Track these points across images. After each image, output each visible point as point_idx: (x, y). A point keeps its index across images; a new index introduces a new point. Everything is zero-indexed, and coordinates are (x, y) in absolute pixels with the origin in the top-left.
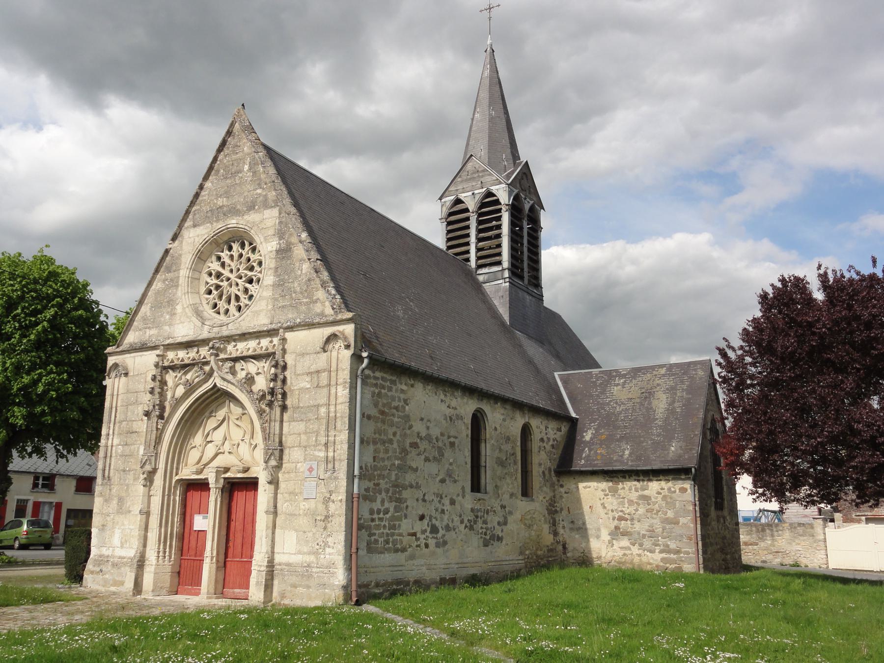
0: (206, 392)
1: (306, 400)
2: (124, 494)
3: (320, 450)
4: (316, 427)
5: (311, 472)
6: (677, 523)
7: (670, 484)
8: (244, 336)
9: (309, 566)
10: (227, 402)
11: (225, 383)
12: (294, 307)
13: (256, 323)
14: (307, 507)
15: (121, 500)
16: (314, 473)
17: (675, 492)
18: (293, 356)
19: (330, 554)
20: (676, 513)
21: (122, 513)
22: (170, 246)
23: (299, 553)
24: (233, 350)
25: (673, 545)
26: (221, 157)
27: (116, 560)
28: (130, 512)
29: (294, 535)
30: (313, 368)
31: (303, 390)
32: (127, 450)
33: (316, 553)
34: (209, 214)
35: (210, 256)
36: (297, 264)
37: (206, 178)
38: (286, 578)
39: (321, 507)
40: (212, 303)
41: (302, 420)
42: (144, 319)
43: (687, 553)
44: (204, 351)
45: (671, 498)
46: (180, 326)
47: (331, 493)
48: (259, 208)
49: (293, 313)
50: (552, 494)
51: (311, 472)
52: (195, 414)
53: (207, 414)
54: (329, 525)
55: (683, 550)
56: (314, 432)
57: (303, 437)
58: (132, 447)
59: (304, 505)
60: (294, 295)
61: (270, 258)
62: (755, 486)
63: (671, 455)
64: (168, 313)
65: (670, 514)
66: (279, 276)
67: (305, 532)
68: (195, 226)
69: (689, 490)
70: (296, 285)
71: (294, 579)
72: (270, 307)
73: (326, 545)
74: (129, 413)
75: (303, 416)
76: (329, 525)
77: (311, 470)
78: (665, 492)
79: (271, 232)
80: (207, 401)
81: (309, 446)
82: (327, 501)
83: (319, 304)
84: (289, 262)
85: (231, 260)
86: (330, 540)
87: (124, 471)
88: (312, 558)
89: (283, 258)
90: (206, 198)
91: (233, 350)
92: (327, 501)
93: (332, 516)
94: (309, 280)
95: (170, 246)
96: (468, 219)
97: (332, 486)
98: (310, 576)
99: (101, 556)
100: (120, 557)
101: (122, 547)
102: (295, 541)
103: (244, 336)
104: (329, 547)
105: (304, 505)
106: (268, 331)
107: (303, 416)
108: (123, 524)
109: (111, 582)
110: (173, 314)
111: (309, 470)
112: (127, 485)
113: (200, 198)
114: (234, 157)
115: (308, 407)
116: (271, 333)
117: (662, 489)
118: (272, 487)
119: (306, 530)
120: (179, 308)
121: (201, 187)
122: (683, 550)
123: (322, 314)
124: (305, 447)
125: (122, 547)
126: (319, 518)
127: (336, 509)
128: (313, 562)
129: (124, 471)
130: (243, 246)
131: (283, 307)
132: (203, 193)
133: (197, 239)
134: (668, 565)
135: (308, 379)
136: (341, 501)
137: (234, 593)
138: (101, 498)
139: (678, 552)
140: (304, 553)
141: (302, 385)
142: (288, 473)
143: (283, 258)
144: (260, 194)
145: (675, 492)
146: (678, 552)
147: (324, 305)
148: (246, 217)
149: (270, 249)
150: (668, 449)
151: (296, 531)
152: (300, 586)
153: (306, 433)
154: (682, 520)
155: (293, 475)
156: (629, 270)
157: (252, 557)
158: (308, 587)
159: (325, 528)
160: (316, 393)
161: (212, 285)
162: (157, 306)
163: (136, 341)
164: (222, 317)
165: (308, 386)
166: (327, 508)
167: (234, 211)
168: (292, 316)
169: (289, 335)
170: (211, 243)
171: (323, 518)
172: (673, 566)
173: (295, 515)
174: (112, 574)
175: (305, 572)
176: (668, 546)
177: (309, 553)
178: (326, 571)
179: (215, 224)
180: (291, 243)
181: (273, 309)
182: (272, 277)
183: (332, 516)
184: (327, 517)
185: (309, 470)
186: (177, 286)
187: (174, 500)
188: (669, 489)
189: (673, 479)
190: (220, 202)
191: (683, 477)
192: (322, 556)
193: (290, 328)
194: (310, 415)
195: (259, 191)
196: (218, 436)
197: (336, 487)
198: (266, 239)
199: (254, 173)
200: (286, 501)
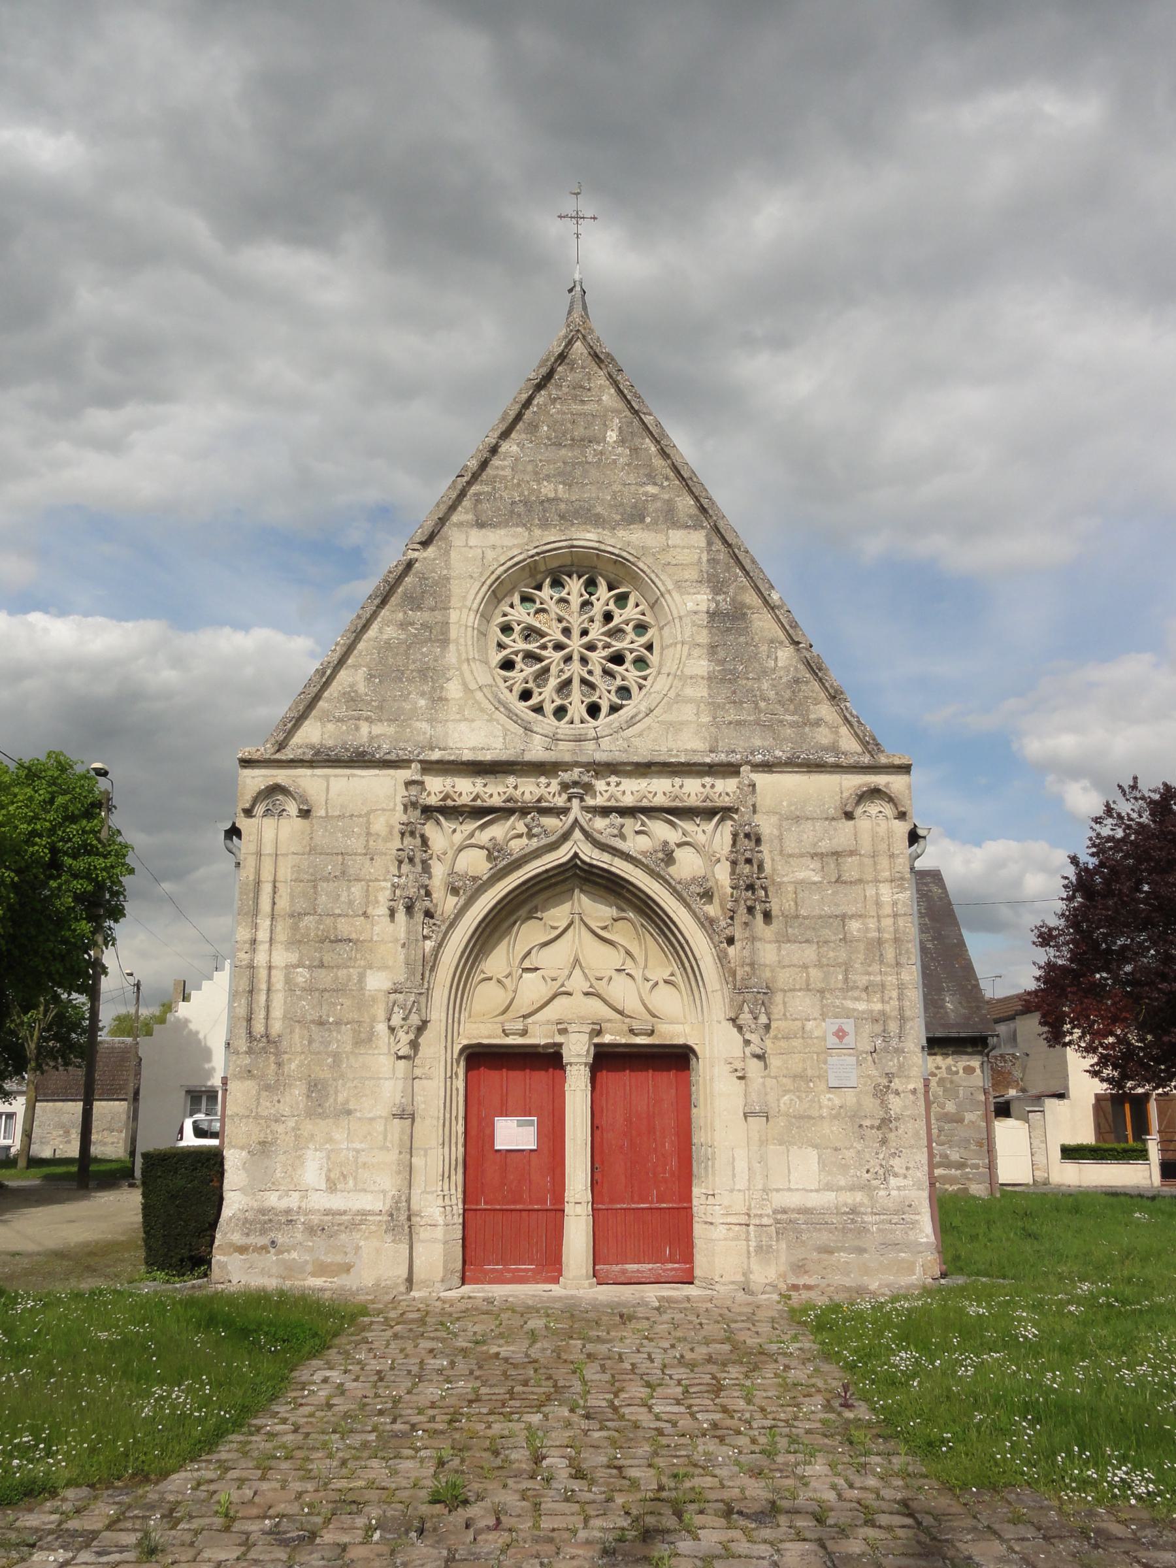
0: (547, 871)
1: (813, 904)
2: (325, 1074)
3: (857, 999)
4: (843, 955)
5: (841, 1038)
6: (960, 1120)
7: (950, 1060)
8: (645, 769)
9: (853, 1211)
10: (577, 891)
11: (606, 857)
12: (767, 727)
13: (671, 744)
14: (837, 1102)
15: (316, 1089)
16: (849, 1040)
17: (957, 1073)
18: (774, 819)
19: (899, 1188)
20: (958, 1105)
21: (323, 1116)
22: (416, 554)
23: (829, 1188)
24: (606, 790)
25: (955, 1156)
26: (540, 399)
27: (315, 1219)
28: (349, 1112)
29: (813, 1154)
30: (825, 846)
32: (325, 978)
33: (866, 1187)
34: (520, 509)
35: (510, 592)
36: (764, 648)
37: (505, 435)
38: (804, 1237)
39: (870, 1104)
40: (517, 689)
41: (807, 941)
42: (351, 698)
43: (976, 1167)
45: (952, 1082)
46: (463, 726)
47: (890, 1076)
48: (655, 522)
49: (764, 739)
51: (841, 1038)
52: (504, 913)
53: (523, 912)
54: (891, 1136)
55: (969, 1162)
56: (839, 965)
57: (813, 972)
58: (342, 973)
59: (830, 1100)
60: (762, 704)
61: (694, 624)
62: (22, 1045)
63: (952, 1015)
64: (423, 694)
65: (950, 1107)
66: (722, 662)
67: (836, 1149)
68: (481, 525)
69: (978, 1071)
70: (765, 686)
71: (825, 1238)
72: (705, 719)
73: (889, 1172)
74: (323, 898)
75: (810, 934)
76: (891, 1136)
77: (840, 1034)
78: (943, 1073)
79: (691, 574)
80: (541, 886)
81: (832, 991)
82: (882, 1092)
83: (823, 730)
84: (742, 639)
85: (564, 608)
86: (896, 1162)
87: (321, 1023)
88: (859, 1197)
89: (728, 630)
90: (508, 472)
91: (606, 790)
92: (882, 1092)
93: (897, 1119)
94: (797, 681)
95: (416, 554)
97: (892, 1065)
98: (863, 1230)
99: (263, 1211)
100: (327, 1212)
101: (332, 1187)
102: (815, 1167)
103: (645, 769)
104: (896, 1175)
105: (830, 1100)
106: (711, 766)
107: (810, 934)
108: (330, 1140)
109: (309, 1268)
110: (438, 700)
111: (836, 1034)
113: (489, 471)
114: (576, 407)
115: (821, 917)
117: (938, 1068)
119: (838, 1145)
120: (453, 690)
121: (494, 450)
122: (969, 1162)
123: (834, 749)
124: (822, 991)
125: (332, 1187)
126: (867, 1123)
127: (905, 1107)
128: (861, 1205)
129: (321, 1023)
130: (591, 584)
131: (739, 723)
132: (496, 462)
133: (490, 555)
134: (947, 1186)
135: (815, 864)
136: (914, 1092)
137: (624, 1272)
138: (249, 1084)
139: (961, 1166)
140: (840, 1189)
141: (801, 875)
142: (787, 1038)
143: (728, 630)
144: (655, 497)
145: (957, 1073)
146: (961, 1166)
147: (837, 733)
148: (621, 533)
149: (691, 606)
150: (943, 1007)
151: (815, 1146)
152: (840, 1249)
153: (819, 965)
154: (969, 1117)
155: (797, 1043)
156: (169, 676)
157: (690, 1201)
158: (861, 1250)
159: (884, 1142)
160: (835, 893)
161: (516, 653)
162: (386, 673)
163: (330, 743)
164: (549, 722)
165: (817, 879)
166: (883, 1104)
167: (588, 516)
168: (759, 744)
169: (762, 779)
170: (523, 568)
171: (877, 1123)
172: (955, 1187)
173: (810, 1117)
174: (310, 1250)
176: (947, 1156)
177: (852, 1189)
178: (895, 1219)
179: (537, 532)
180: (743, 605)
181: (714, 723)
182: (704, 663)
183: (897, 1119)
185: (836, 1034)
186: (445, 642)
187: (457, 1089)
188: (949, 1068)
189: (953, 1053)
190: (548, 489)
191: (970, 1050)
192: (882, 1193)
193: (766, 767)
194: (827, 933)
195: (652, 489)
196: (554, 958)
197: (901, 1066)
198: (678, 585)
199: (635, 450)
200: (786, 1092)
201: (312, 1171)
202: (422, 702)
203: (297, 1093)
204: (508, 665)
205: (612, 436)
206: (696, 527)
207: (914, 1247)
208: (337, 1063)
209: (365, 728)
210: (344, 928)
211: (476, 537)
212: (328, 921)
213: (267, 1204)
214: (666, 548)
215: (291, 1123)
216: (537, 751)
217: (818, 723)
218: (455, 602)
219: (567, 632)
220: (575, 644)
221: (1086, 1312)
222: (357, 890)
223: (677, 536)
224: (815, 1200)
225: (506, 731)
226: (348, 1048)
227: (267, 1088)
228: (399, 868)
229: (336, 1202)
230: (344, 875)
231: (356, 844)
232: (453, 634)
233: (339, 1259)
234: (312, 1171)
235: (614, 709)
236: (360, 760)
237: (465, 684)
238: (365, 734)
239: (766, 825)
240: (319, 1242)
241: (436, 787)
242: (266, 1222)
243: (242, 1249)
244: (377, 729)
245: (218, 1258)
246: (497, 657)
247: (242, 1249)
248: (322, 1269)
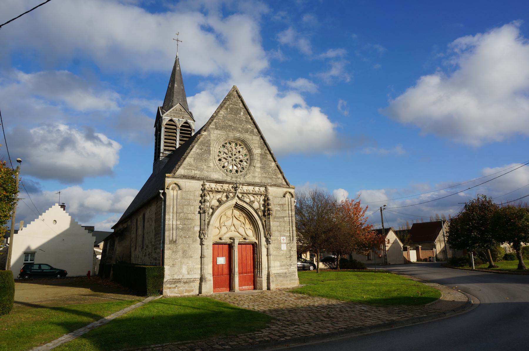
1: (279, 214)
12: (271, 178)
15: (184, 252)
30: (280, 203)
31: (277, 210)
39: (288, 253)
44: (226, 187)
46: (214, 173)
47: (291, 248)
50: (57, 208)
57: (279, 228)
58: (189, 226)
82: (290, 250)
88: (286, 270)
92: (290, 250)
96: (166, 124)
101: (188, 274)
108: (188, 263)
112: (189, 244)
116: (260, 185)
118: (402, 262)
125: (188, 274)
138: (170, 251)
175: (284, 276)
184: (291, 256)
201: (184, 270)
202: (205, 167)
203: (180, 253)
204: (220, 160)
205: (242, 114)
206: (258, 136)
207: (295, 280)
208: (189, 246)
209: (193, 171)
210: (190, 216)
211: (216, 132)
212: (186, 215)
213: (175, 278)
214: (252, 140)
215: (179, 260)
216: (229, 179)
217: (279, 178)
218: (212, 145)
219: (235, 155)
220: (234, 157)
221: (384, 250)
222: (192, 208)
223: (254, 137)
224: (279, 272)
225: (223, 175)
226: (191, 242)
227: (173, 252)
228: (266, 201)
229: (189, 277)
230: (189, 204)
231: (192, 197)
232: (211, 152)
233: (191, 289)
234: (184, 270)
235: (241, 171)
236: (193, 178)
237: (214, 164)
238: (193, 173)
239: (270, 197)
240: (186, 285)
241: (208, 185)
242: (176, 282)
243: (170, 288)
244: (196, 172)
245: (164, 291)
246: (218, 158)
247: (170, 288)
248: (187, 291)
